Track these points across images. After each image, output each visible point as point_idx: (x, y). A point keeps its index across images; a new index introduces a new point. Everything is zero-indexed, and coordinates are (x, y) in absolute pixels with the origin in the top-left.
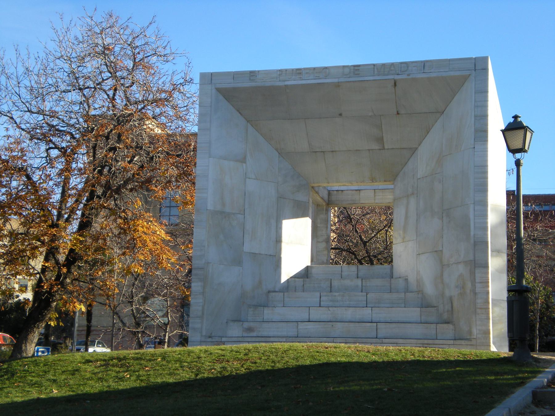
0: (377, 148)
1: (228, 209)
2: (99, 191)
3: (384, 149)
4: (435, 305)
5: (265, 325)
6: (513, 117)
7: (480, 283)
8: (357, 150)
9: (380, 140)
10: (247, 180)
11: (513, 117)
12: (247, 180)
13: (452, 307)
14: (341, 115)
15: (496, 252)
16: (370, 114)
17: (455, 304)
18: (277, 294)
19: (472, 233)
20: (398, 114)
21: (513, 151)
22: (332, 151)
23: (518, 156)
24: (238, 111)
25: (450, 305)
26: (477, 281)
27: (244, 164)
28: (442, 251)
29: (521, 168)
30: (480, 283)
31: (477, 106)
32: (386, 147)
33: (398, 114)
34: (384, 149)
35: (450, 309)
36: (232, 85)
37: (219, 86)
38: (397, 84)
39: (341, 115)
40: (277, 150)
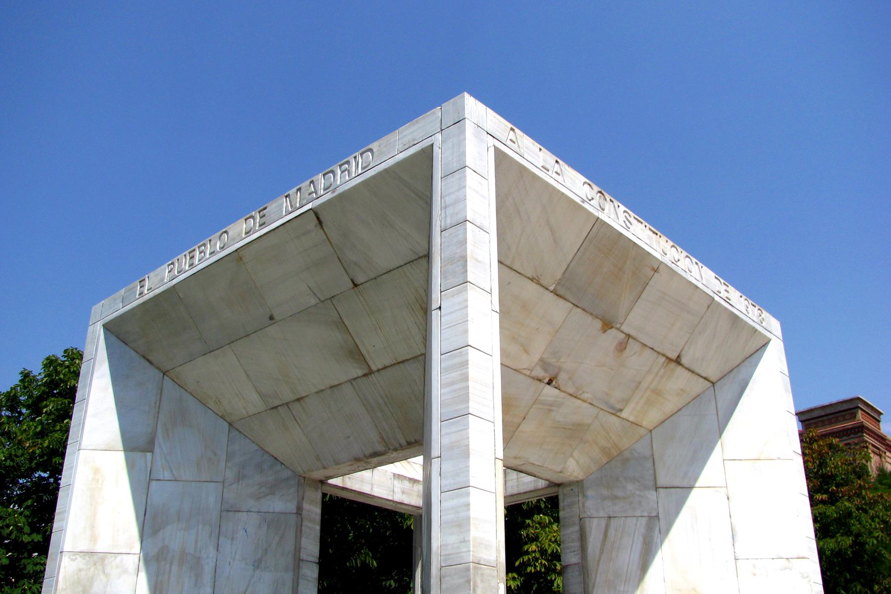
0: (360, 373)
9: (356, 354)
15: (96, 558)
20: (356, 285)
22: (298, 400)
24: (144, 357)
27: (149, 455)
33: (356, 285)
34: (371, 372)
39: (271, 318)
40: (222, 417)
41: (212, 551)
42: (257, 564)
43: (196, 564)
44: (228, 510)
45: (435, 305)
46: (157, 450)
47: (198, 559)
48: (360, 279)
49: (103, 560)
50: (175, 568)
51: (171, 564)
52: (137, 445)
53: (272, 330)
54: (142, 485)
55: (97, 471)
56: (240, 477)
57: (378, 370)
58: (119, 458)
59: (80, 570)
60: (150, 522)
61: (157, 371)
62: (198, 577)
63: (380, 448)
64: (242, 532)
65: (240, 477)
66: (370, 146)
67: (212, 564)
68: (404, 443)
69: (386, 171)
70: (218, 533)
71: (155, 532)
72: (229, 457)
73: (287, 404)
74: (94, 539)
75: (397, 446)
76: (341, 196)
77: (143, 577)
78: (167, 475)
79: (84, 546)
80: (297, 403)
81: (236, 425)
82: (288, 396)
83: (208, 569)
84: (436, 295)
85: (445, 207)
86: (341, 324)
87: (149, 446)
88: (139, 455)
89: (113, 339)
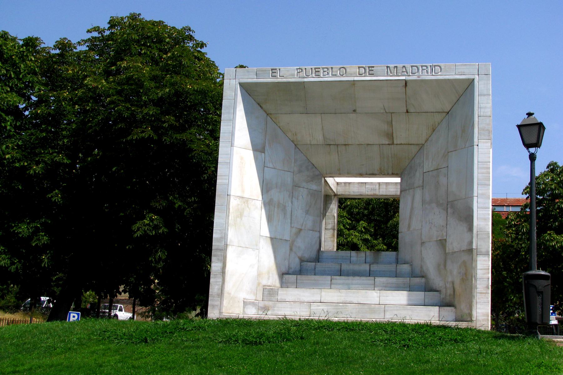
0: (387, 143)
1: (246, 195)
2: (405, 268)
3: (393, 144)
4: (438, 289)
5: (279, 305)
6: (527, 114)
7: (481, 269)
8: (368, 144)
9: (390, 136)
10: (266, 168)
11: (527, 114)
12: (266, 168)
13: (454, 292)
14: (354, 111)
15: (245, 200)
16: (382, 111)
17: (457, 287)
18: (290, 276)
19: (475, 223)
20: (407, 112)
21: (528, 146)
22: (345, 145)
23: (532, 150)
24: (259, 104)
25: (452, 289)
26: (478, 268)
27: (263, 154)
28: (446, 240)
29: (536, 162)
30: (481, 269)
31: (480, 108)
32: (395, 143)
33: (407, 112)
34: (393, 144)
35: (452, 293)
36: (255, 80)
37: (243, 81)
38: (408, 84)
39: (354, 111)
40: (293, 141)
41: (290, 203)
42: (307, 212)
43: (284, 209)
44: (296, 186)
45: (475, 143)
46: (266, 152)
47: (285, 207)
48: (411, 110)
49: (247, 201)
50: (276, 209)
51: (274, 207)
52: (258, 149)
53: (353, 116)
54: (261, 168)
55: (242, 159)
56: (300, 171)
57: (397, 144)
58: (251, 153)
59: (238, 205)
60: (266, 187)
61: (264, 113)
62: (285, 214)
63: (376, 172)
64: (301, 197)
65: (300, 171)
66: (442, 65)
67: (290, 210)
68: (390, 173)
69: (449, 80)
70: (292, 196)
71: (267, 191)
72: (296, 160)
73: (337, 145)
74: (243, 191)
75: (386, 172)
76: (423, 81)
77: (263, 211)
78: (271, 166)
79: (239, 194)
80: (344, 147)
81: (298, 146)
82: (341, 141)
83: (289, 209)
84: (476, 140)
85: (480, 108)
86: (390, 124)
87: (263, 151)
88: (258, 153)
89: (244, 91)
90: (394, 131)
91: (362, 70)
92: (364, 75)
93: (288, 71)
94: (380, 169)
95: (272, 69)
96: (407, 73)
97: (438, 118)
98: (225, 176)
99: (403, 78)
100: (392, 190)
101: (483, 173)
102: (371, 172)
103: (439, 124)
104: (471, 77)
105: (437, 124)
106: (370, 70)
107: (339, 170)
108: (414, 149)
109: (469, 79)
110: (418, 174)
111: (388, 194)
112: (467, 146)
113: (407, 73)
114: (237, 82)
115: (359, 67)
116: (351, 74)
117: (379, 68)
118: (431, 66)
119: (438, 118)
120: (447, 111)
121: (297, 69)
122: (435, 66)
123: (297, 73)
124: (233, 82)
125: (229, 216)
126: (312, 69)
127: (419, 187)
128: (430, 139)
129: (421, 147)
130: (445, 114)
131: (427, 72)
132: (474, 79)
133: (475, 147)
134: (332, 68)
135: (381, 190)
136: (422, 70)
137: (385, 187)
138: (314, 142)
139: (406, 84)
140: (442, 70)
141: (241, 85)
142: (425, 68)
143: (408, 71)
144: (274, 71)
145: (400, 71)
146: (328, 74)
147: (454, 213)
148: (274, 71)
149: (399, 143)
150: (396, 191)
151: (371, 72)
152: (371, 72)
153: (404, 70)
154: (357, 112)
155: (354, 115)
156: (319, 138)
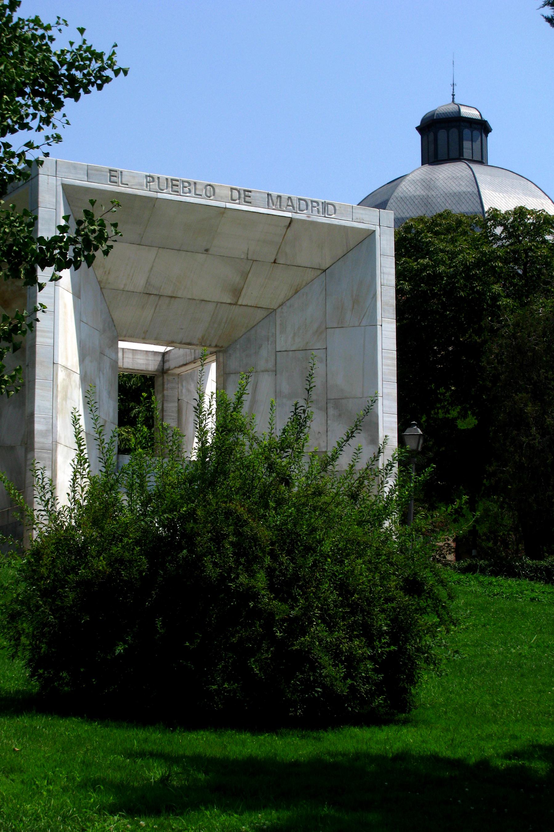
0: (229, 301)
9: (237, 292)
14: (207, 250)
16: (242, 256)
20: (275, 262)
31: (384, 273)
34: (236, 304)
39: (207, 250)
40: (100, 282)
45: (379, 323)
46: (82, 298)
53: (201, 257)
63: (195, 341)
65: (104, 331)
84: (379, 317)
86: (245, 275)
90: (246, 286)
91: (236, 194)
92: (238, 201)
93: (134, 177)
94: (203, 338)
95: (110, 170)
96: (293, 207)
97: (311, 274)
98: (48, 332)
99: (289, 215)
100: (141, 361)
101: (388, 366)
102: (188, 341)
103: (307, 284)
104: (372, 228)
105: (304, 284)
106: (246, 196)
107: (146, 332)
108: (261, 314)
109: (368, 230)
110: (264, 352)
111: (136, 367)
112: (364, 323)
113: (293, 207)
114: (59, 183)
115: (232, 189)
116: (222, 197)
117: (258, 194)
118: (323, 203)
119: (311, 274)
120: (324, 268)
121: (147, 176)
122: (328, 204)
123: (147, 182)
124: (52, 180)
125: (57, 397)
126: (167, 179)
127: (267, 371)
128: (288, 304)
129: (271, 312)
130: (319, 272)
131: (318, 212)
132: (374, 231)
133: (379, 327)
134: (195, 183)
135: (126, 360)
136: (313, 207)
137: (130, 356)
138: (130, 288)
139: (290, 224)
140: (337, 212)
141: (66, 188)
142: (315, 204)
143: (295, 206)
144: (113, 173)
145: (284, 203)
146: (190, 192)
147: (340, 415)
148: (113, 173)
149: (244, 304)
150: (147, 364)
151: (248, 199)
152: (248, 199)
153: (290, 203)
154: (210, 252)
155: (204, 256)
156: (139, 283)
